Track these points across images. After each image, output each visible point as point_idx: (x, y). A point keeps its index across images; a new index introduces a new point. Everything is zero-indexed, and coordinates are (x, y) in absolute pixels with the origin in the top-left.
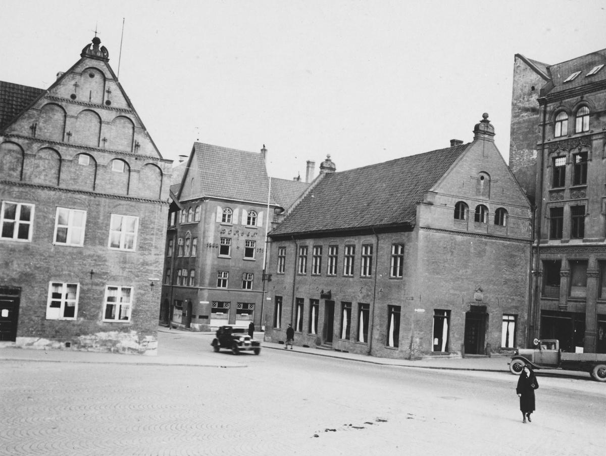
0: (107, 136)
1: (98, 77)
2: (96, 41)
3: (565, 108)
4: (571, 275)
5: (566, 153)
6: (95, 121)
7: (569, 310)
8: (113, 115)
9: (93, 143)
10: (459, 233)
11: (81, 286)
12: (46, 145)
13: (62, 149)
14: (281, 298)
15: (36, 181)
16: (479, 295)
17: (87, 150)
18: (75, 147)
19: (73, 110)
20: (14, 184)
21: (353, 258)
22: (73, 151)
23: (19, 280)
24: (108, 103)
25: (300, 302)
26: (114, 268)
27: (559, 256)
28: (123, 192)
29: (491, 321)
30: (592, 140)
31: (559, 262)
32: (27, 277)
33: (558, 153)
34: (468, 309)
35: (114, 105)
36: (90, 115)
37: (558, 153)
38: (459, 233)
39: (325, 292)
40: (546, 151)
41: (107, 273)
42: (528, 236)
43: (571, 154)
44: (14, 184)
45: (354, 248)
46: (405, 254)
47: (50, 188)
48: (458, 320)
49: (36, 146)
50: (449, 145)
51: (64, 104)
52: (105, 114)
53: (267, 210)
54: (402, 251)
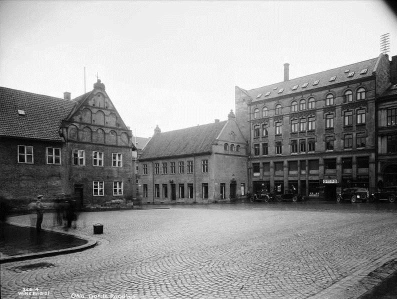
0: (108, 121)
1: (101, 96)
2: (99, 81)
3: (365, 87)
4: (263, 168)
5: (259, 124)
7: (264, 180)
10: (227, 155)
12: (86, 126)
14: (146, 185)
15: (84, 140)
16: (234, 177)
17: (101, 127)
18: (96, 126)
19: (94, 111)
20: (76, 142)
21: (192, 166)
22: (96, 128)
23: (83, 182)
25: (157, 186)
26: (116, 175)
27: (258, 162)
28: (114, 144)
29: (238, 186)
31: (259, 164)
32: (85, 180)
33: (348, 110)
34: (231, 183)
37: (348, 110)
38: (227, 155)
39: (171, 180)
40: (252, 124)
41: (113, 177)
42: (244, 154)
43: (356, 110)
44: (76, 142)
45: (174, 164)
46: (208, 164)
47: (89, 143)
48: (228, 187)
49: (82, 126)
51: (90, 108)
54: (174, 165)
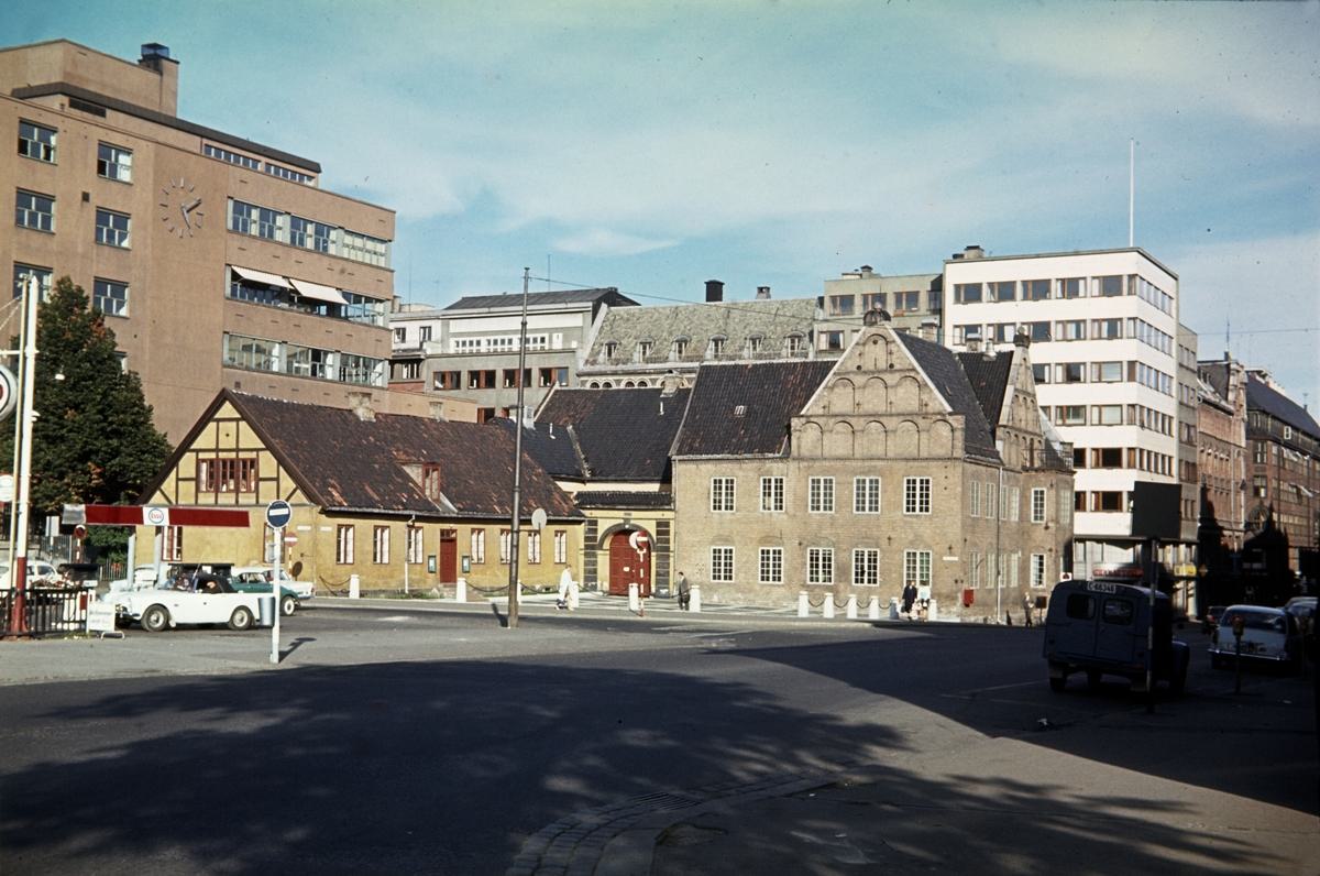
6: (850, 389)
8: (897, 376)
9: (882, 409)
11: (1140, 583)
13: (853, 421)
24: (892, 366)
30: (799, 455)
35: (897, 367)
36: (908, 381)
50: (146, 404)
52: (891, 379)
53: (409, 585)
